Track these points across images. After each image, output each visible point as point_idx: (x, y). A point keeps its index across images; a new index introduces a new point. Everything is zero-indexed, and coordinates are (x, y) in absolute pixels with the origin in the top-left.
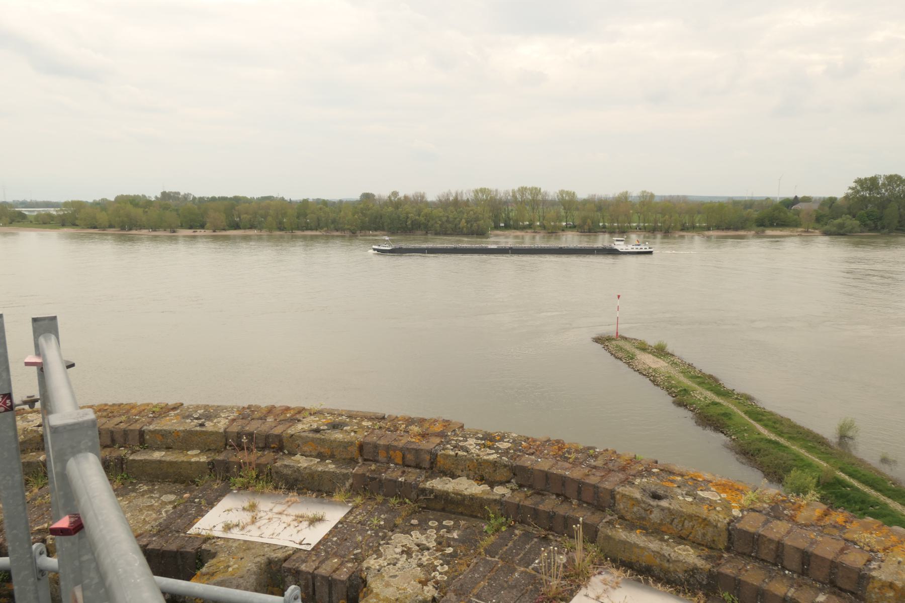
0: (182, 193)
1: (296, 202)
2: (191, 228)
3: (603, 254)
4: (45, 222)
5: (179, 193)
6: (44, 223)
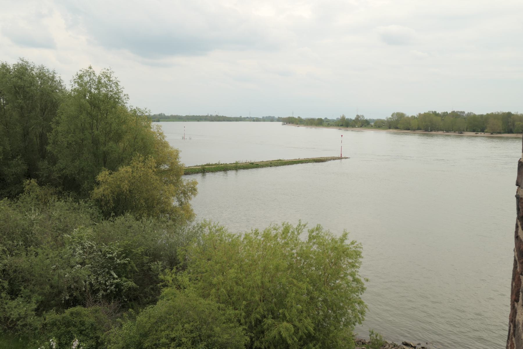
0: (466, 113)
1: (413, 118)
2: (474, 131)
3: (291, 164)
4: (380, 125)
5: (464, 112)
6: (379, 127)
